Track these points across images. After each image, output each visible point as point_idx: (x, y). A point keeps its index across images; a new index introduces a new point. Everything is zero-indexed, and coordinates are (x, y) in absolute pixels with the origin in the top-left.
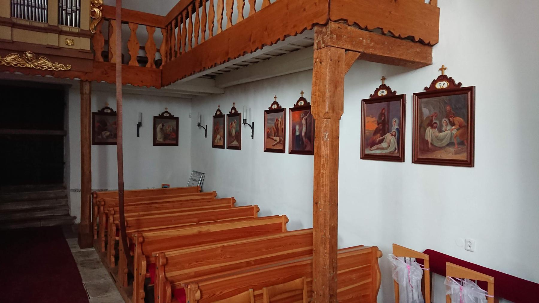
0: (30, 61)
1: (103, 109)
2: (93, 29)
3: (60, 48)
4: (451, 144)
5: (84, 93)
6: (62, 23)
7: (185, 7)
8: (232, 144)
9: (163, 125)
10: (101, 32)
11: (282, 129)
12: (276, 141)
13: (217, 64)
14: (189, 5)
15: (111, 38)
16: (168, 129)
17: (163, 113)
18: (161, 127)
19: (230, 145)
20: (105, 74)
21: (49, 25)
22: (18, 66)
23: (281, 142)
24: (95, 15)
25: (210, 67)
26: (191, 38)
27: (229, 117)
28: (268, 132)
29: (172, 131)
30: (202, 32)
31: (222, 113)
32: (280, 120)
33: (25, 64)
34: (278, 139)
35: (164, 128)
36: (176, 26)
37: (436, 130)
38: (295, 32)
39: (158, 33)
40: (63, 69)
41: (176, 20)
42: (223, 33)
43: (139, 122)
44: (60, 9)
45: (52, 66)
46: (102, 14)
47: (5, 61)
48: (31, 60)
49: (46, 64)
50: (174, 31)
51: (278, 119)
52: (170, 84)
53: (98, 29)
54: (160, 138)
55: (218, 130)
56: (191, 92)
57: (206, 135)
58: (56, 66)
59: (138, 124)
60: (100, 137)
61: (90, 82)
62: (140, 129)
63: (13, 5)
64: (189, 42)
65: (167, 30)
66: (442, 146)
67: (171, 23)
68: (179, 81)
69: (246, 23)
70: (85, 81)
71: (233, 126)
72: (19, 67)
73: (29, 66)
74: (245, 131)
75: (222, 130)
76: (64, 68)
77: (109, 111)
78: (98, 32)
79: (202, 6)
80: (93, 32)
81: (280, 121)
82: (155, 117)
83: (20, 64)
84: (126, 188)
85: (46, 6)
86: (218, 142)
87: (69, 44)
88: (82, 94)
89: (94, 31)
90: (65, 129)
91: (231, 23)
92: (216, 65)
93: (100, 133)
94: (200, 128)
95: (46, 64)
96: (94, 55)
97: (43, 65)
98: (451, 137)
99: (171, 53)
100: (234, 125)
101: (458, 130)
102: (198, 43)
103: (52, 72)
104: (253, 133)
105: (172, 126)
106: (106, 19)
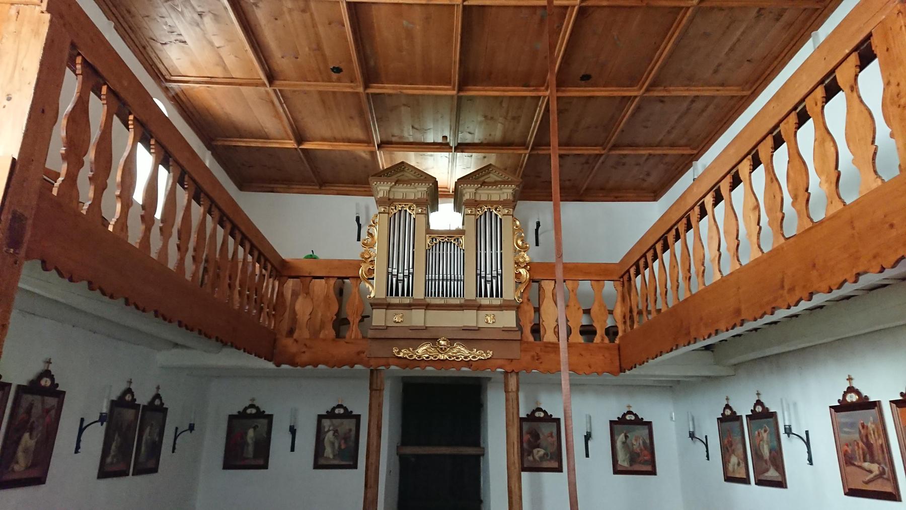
0: (443, 350)
1: (534, 412)
2: (519, 297)
3: (479, 329)
5: (510, 390)
6: (481, 296)
7: (650, 245)
8: (766, 474)
9: (626, 437)
10: (529, 300)
11: (882, 445)
12: (870, 472)
13: (719, 331)
14: (657, 242)
15: (542, 306)
16: (635, 443)
17: (624, 415)
18: (624, 439)
19: (762, 477)
20: (537, 360)
21: (466, 300)
22: (430, 359)
23: (885, 476)
24: (521, 278)
25: (706, 337)
26: (665, 292)
27: (750, 419)
28: (846, 451)
29: (642, 448)
30: (683, 280)
31: (734, 413)
32: (871, 426)
33: (438, 355)
34: (875, 468)
35: (628, 441)
36: (638, 273)
38: (880, 267)
39: (609, 287)
40: (483, 358)
41: (636, 267)
42: (724, 280)
43: (587, 432)
44: (479, 277)
45: (469, 354)
46: (530, 275)
47: (417, 353)
48: (445, 349)
49: (462, 352)
50: (635, 282)
51: (865, 424)
52: (635, 367)
53: (525, 296)
54: (623, 462)
55: (731, 446)
56: (667, 376)
57: (708, 456)
58: (474, 354)
59: (586, 434)
60: (531, 458)
61: (517, 373)
62: (590, 443)
63: (427, 282)
64: (662, 298)
65: (623, 282)
67: (628, 271)
68: (651, 361)
69: (766, 261)
70: (510, 373)
71: (763, 437)
72: (431, 360)
73: (442, 358)
74: (792, 451)
75: (740, 446)
76: (484, 356)
77: (542, 415)
78: (526, 300)
79: (680, 238)
80: (518, 300)
81: (871, 429)
82: (612, 422)
83: (432, 356)
85: (462, 276)
86: (734, 469)
87: (489, 322)
88: (507, 391)
89: (520, 300)
90: (482, 445)
91: (738, 262)
92: (717, 332)
93: (530, 453)
94: (694, 442)
95: (462, 352)
96: (522, 333)
97: (458, 354)
99: (631, 318)
100: (765, 435)
102: (679, 299)
103: (469, 364)
104: (809, 452)
105: (641, 438)
106: (534, 281)
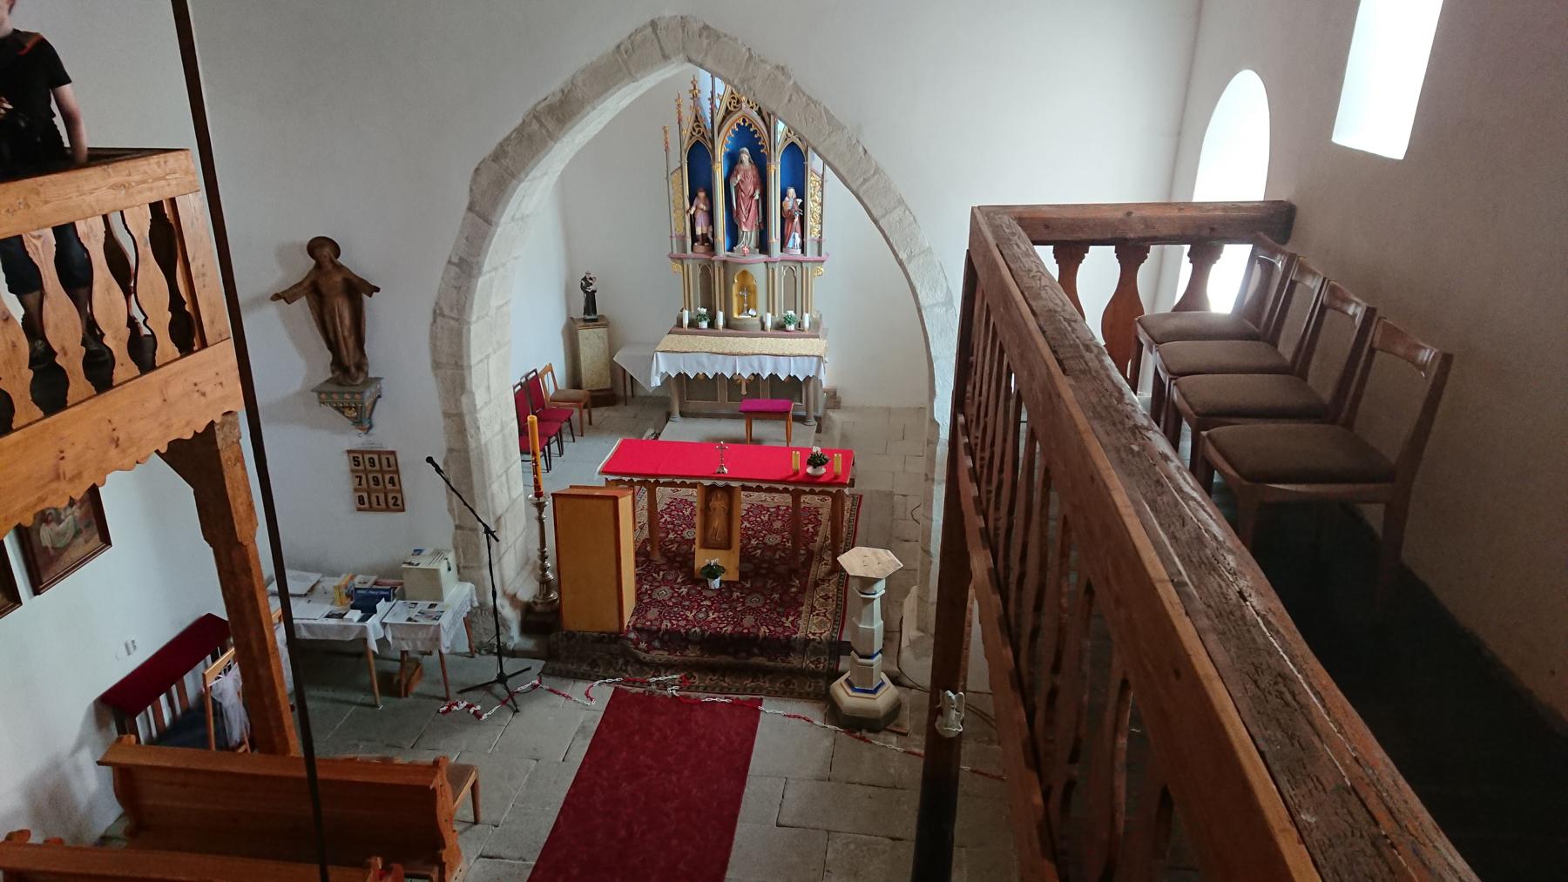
4: (78, 533)
37: (53, 525)
66: (68, 541)
84: (316, 868)
98: (75, 521)
101: (80, 508)
